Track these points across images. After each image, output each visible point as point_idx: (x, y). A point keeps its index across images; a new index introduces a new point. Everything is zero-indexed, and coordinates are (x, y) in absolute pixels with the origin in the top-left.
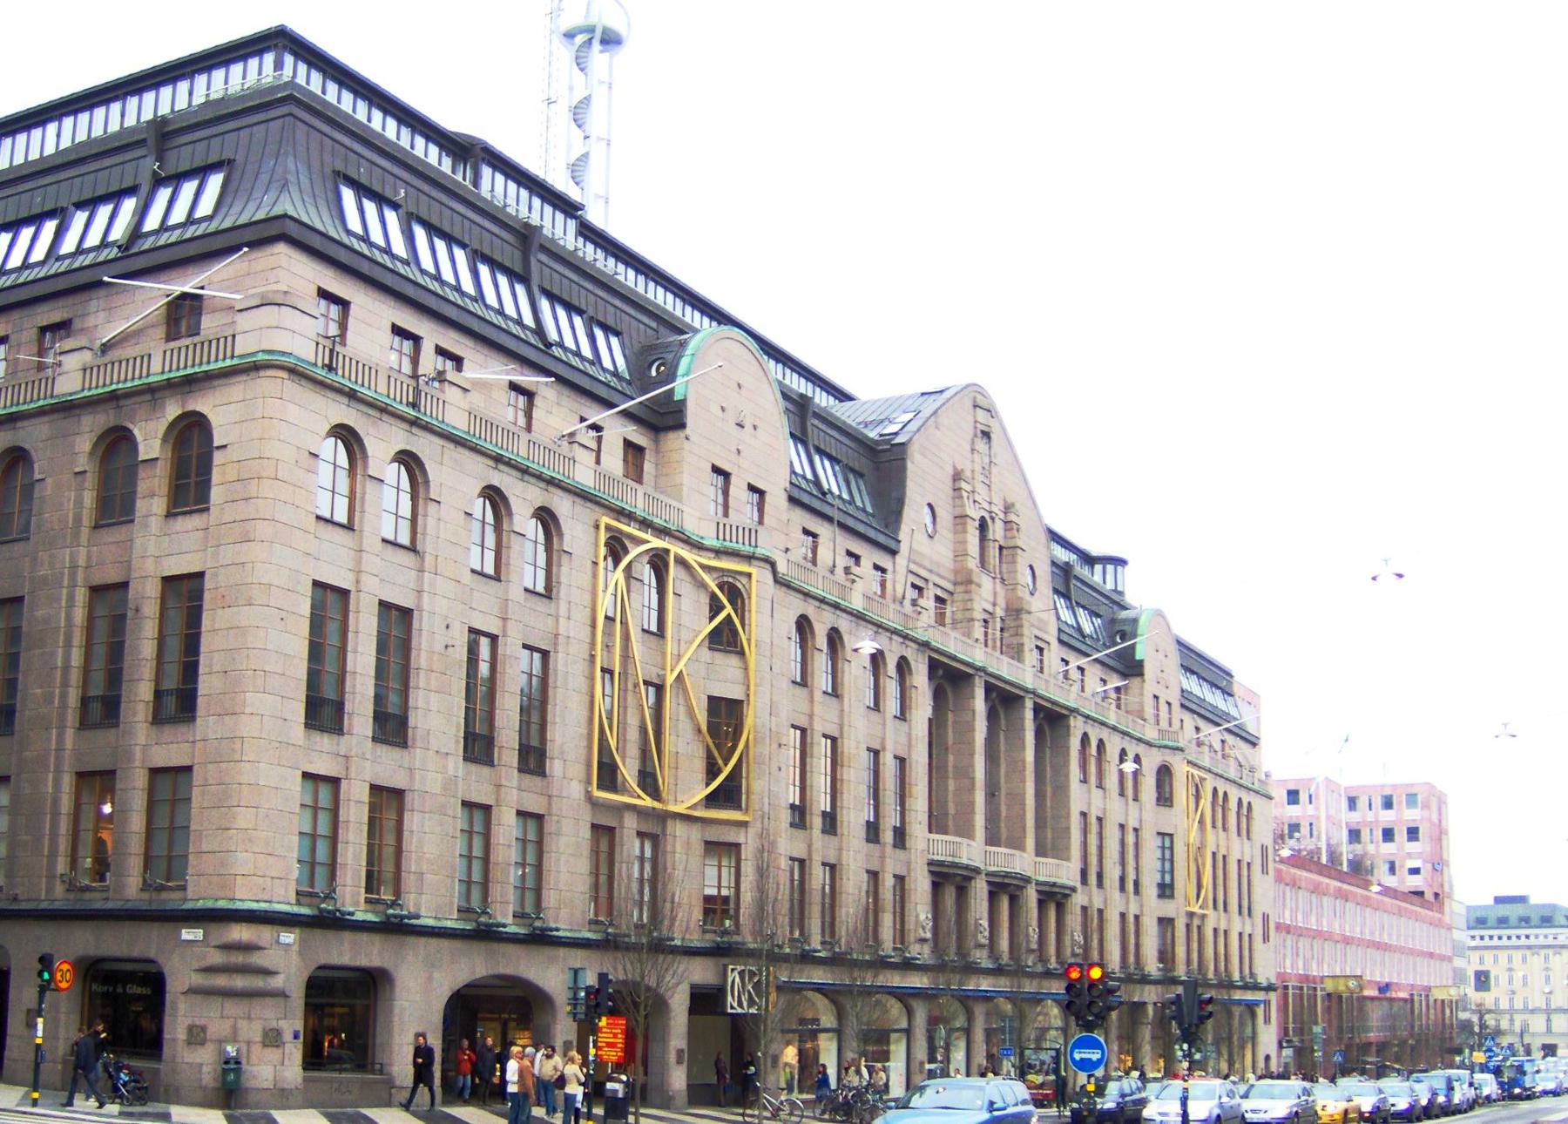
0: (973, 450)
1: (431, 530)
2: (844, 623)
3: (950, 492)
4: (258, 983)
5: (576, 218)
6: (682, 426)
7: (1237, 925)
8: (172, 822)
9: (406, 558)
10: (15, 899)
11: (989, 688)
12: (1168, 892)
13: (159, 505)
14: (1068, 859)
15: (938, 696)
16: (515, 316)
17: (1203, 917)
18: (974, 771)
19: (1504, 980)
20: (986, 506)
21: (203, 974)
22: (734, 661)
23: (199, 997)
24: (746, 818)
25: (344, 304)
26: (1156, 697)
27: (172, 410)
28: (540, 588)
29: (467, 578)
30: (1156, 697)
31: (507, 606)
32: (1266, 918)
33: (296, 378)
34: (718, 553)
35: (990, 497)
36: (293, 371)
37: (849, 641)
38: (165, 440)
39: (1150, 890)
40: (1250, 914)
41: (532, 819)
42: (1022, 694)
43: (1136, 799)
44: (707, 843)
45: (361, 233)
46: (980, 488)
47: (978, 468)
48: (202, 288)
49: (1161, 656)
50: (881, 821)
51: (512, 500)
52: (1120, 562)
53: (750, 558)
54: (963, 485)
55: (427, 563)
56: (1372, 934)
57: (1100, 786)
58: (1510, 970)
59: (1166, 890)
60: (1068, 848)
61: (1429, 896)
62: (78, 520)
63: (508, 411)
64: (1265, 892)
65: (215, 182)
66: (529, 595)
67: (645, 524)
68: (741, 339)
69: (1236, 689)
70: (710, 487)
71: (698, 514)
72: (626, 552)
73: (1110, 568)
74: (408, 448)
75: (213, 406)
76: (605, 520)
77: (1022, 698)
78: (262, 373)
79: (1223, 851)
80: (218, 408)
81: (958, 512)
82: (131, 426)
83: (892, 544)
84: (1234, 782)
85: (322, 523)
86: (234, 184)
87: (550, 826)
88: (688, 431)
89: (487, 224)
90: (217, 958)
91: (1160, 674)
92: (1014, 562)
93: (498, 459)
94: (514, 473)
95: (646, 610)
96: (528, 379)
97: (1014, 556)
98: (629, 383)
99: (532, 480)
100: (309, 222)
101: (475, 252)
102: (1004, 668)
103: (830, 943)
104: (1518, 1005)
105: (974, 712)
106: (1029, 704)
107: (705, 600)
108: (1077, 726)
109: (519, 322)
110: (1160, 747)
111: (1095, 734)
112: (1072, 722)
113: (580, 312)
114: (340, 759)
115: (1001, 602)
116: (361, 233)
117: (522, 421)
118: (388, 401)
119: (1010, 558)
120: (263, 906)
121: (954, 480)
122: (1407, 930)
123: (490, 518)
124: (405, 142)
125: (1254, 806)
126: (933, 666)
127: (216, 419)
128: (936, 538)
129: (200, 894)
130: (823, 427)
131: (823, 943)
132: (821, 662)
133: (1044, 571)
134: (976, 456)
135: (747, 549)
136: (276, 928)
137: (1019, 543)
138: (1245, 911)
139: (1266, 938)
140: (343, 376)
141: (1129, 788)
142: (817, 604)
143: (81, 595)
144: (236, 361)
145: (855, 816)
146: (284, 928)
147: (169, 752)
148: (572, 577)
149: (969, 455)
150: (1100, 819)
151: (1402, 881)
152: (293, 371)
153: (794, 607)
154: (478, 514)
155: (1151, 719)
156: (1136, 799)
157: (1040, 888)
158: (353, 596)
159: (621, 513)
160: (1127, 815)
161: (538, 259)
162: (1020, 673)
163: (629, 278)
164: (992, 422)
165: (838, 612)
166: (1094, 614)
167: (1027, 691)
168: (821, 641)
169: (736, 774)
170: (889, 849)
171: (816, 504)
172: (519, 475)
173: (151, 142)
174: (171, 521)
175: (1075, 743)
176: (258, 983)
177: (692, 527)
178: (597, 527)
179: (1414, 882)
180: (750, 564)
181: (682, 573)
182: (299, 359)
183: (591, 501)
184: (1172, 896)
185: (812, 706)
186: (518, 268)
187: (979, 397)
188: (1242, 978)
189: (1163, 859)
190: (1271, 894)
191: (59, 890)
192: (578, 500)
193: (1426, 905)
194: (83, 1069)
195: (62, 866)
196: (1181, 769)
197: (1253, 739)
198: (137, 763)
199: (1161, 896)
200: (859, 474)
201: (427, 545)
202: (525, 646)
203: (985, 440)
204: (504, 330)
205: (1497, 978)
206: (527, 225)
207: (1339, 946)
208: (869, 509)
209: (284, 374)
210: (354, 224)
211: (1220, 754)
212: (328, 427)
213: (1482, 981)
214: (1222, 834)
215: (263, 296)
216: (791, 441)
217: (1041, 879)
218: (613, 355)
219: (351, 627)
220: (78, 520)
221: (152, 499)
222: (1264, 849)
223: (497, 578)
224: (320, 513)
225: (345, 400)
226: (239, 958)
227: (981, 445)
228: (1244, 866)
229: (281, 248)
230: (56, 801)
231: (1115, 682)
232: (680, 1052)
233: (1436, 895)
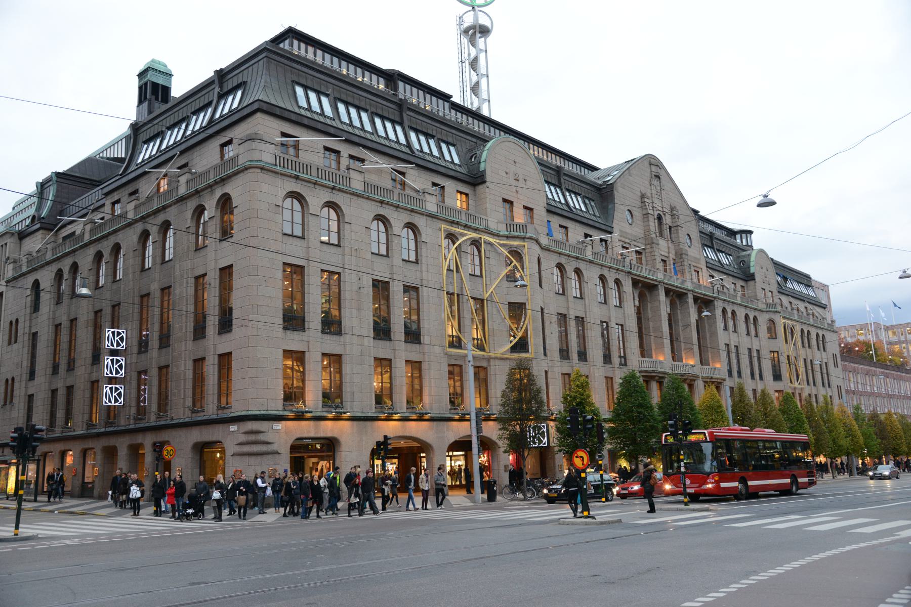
0: (651, 184)
1: (424, 254)
2: (736, 308)
4: (263, 448)
5: (447, 102)
6: (485, 182)
7: (822, 392)
9: (563, 297)
10: (172, 419)
11: (668, 292)
15: (672, 304)
16: (395, 139)
18: (662, 328)
20: (661, 209)
21: (239, 446)
23: (239, 457)
25: (566, 228)
27: (218, 193)
28: (578, 296)
29: (369, 256)
31: (393, 268)
32: (839, 388)
33: (265, 172)
34: (508, 237)
35: (662, 205)
36: (262, 169)
37: (828, 338)
38: (217, 208)
40: (829, 386)
41: (416, 365)
42: (686, 292)
45: (429, 152)
46: (656, 201)
47: (654, 192)
49: (764, 270)
50: (611, 353)
51: (392, 220)
52: (751, 232)
53: (524, 238)
54: (646, 200)
55: (346, 251)
57: (735, 331)
63: (559, 235)
64: (837, 375)
65: (239, 94)
66: (404, 262)
67: (466, 227)
68: (514, 141)
69: (813, 284)
70: (501, 209)
71: (496, 221)
72: (458, 239)
73: (744, 236)
74: (331, 200)
75: (233, 189)
76: (444, 226)
78: (248, 171)
79: (810, 357)
80: (233, 189)
81: (645, 212)
82: (204, 204)
83: (609, 229)
84: (813, 325)
85: (375, 255)
86: (246, 92)
87: (425, 366)
89: (379, 100)
90: (243, 438)
91: (764, 279)
92: (677, 233)
93: (382, 202)
94: (392, 208)
95: (557, 285)
96: (401, 166)
97: (677, 230)
98: (460, 166)
99: (402, 210)
100: (336, 126)
101: (372, 113)
102: (675, 282)
105: (659, 301)
109: (560, 202)
110: (767, 312)
112: (716, 303)
113: (580, 195)
114: (305, 342)
115: (673, 252)
116: (429, 152)
117: (565, 238)
118: (318, 179)
119: (675, 232)
120: (263, 412)
121: (641, 198)
123: (559, 274)
124: (327, 63)
126: (635, 283)
127: (233, 196)
128: (633, 225)
129: (237, 409)
130: (571, 180)
133: (695, 235)
134: (653, 187)
135: (522, 234)
136: (271, 422)
137: (679, 224)
138: (827, 385)
140: (284, 167)
142: (567, 258)
144: (239, 167)
146: (275, 422)
147: (224, 344)
149: (649, 187)
150: (737, 347)
152: (262, 169)
153: (554, 259)
154: (555, 273)
157: (704, 380)
158: (306, 269)
160: (752, 344)
161: (563, 178)
162: (686, 282)
163: (345, 69)
164: (659, 171)
165: (579, 261)
168: (730, 315)
171: (721, 269)
172: (394, 209)
173: (217, 81)
175: (719, 312)
176: (263, 448)
177: (493, 226)
180: (524, 241)
181: (489, 248)
182: (266, 163)
183: (435, 218)
185: (568, 304)
186: (397, 119)
187: (652, 160)
192: (428, 218)
194: (455, 472)
196: (780, 322)
197: (824, 306)
201: (345, 243)
202: (617, 324)
203: (657, 179)
204: (438, 164)
206: (558, 167)
207: (885, 399)
208: (456, 161)
209: (259, 171)
210: (303, 103)
212: (403, 224)
215: (248, 135)
216: (546, 185)
217: (704, 375)
218: (452, 155)
219: (421, 302)
222: (834, 356)
223: (417, 262)
224: (373, 251)
225: (294, 180)
226: (252, 438)
227: (655, 182)
228: (824, 367)
231: (740, 283)
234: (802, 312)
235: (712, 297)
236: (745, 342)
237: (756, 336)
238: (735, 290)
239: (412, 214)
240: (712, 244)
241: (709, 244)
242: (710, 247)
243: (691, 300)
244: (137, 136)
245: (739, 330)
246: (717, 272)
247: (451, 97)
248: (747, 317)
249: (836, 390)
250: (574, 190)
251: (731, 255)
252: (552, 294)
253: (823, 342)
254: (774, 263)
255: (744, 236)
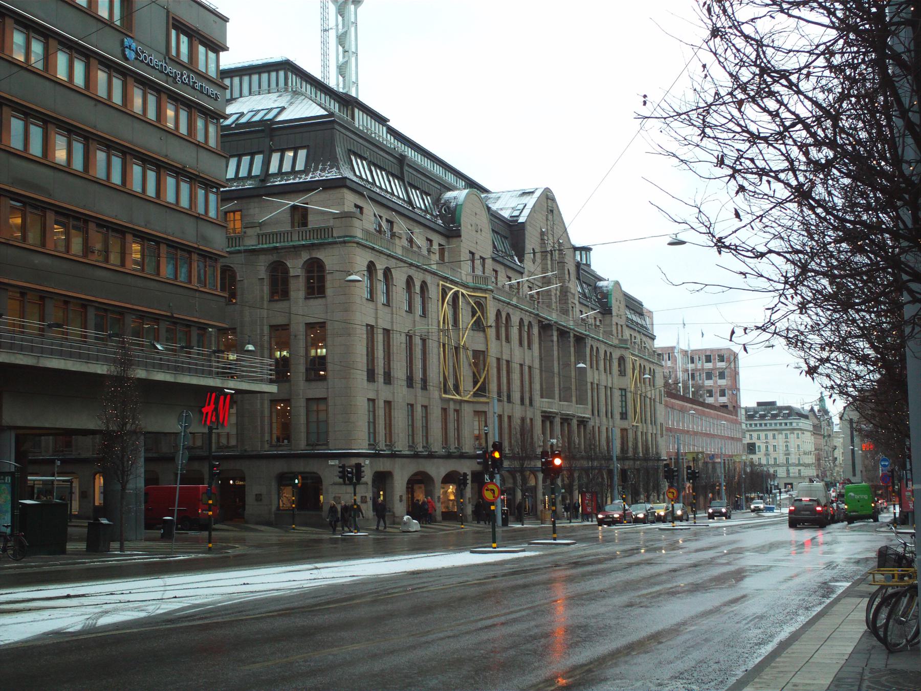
2: (429, 279)
3: (539, 240)
8: (318, 418)
11: (558, 329)
12: (624, 416)
13: (302, 294)
14: (587, 404)
17: (637, 426)
19: (763, 448)
22: (481, 334)
24: (488, 400)
26: (472, 254)
27: (305, 256)
30: (472, 254)
39: (617, 416)
43: (610, 373)
44: (474, 411)
48: (307, 204)
53: (485, 291)
56: (706, 430)
58: (767, 442)
59: (624, 416)
60: (554, 396)
61: (730, 408)
62: (262, 298)
73: (583, 253)
77: (569, 332)
78: (347, 245)
88: (462, 238)
103: (389, 446)
104: (772, 462)
106: (572, 335)
107: (470, 309)
108: (589, 342)
111: (595, 345)
113: (365, 159)
121: (541, 235)
122: (721, 426)
125: (656, 371)
131: (386, 445)
132: (381, 287)
139: (662, 436)
141: (608, 370)
143: (266, 330)
145: (399, 371)
147: (316, 390)
148: (432, 307)
151: (717, 400)
155: (616, 335)
156: (610, 373)
159: (446, 279)
166: (424, 193)
167: (571, 329)
168: (380, 275)
169: (484, 383)
170: (506, 403)
174: (307, 301)
175: (588, 350)
178: (438, 285)
179: (723, 400)
180: (486, 293)
184: (626, 418)
188: (412, 447)
189: (622, 401)
190: (663, 413)
191: (266, 446)
193: (730, 413)
195: (267, 437)
196: (630, 358)
198: (301, 397)
199: (622, 418)
200: (506, 238)
205: (759, 447)
211: (388, 234)
213: (751, 448)
214: (596, 373)
220: (262, 298)
221: (298, 290)
227: (550, 217)
229: (345, 191)
230: (262, 412)
231: (437, 239)
232: (469, 498)
233: (734, 407)
234: (419, 247)
235: (583, 334)
236: (402, 323)
237: (388, 304)
238: (429, 251)
239: (389, 258)
240: (402, 173)
241: (397, 173)
242: (398, 178)
243: (572, 339)
244: (176, 172)
245: (394, 304)
246: (402, 218)
247: (389, 120)
248: (410, 281)
249: (659, 427)
250: (359, 153)
251: (429, 195)
252: (364, 300)
253: (596, 357)
254: (492, 215)
255: (583, 253)
